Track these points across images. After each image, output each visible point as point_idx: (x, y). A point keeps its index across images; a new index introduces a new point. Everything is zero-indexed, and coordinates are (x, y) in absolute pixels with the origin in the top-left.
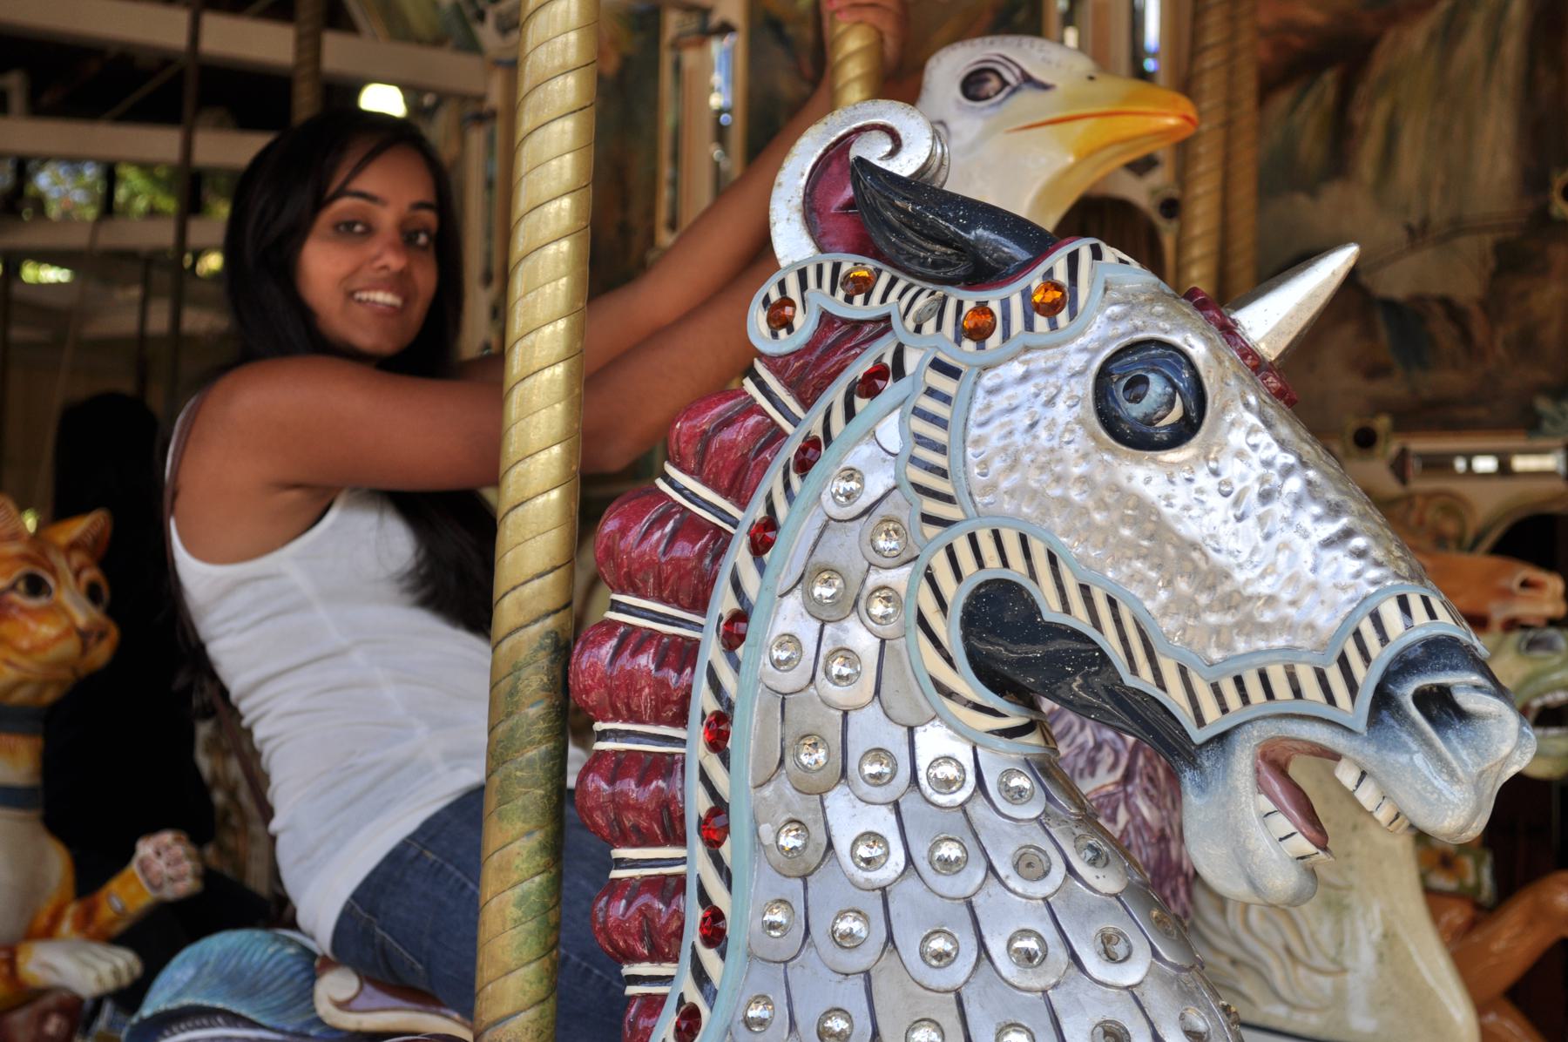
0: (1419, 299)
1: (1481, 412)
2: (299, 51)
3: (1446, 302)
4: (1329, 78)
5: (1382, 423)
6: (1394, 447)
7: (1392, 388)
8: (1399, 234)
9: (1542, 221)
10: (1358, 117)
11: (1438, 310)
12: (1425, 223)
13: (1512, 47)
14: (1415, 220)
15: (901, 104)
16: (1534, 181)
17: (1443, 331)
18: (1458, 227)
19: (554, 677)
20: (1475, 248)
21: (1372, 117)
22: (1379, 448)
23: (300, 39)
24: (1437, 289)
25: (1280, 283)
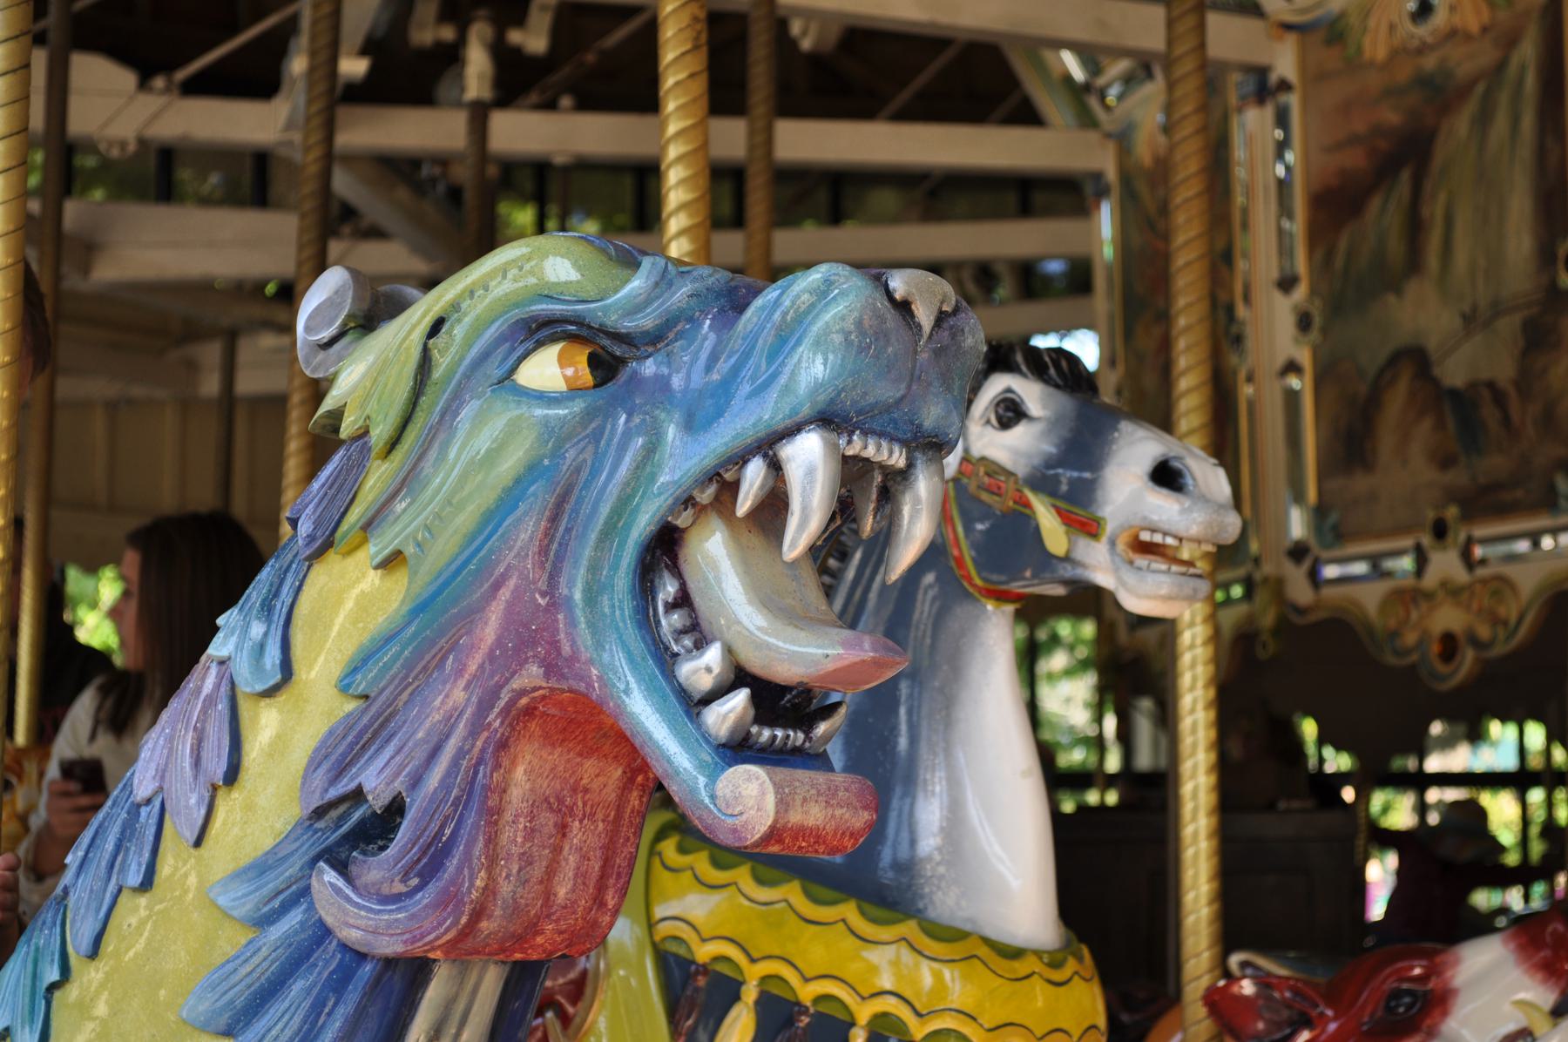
0: (1473, 385)
1: (1519, 493)
2: (751, 148)
3: (1491, 385)
4: (1405, 176)
5: (1452, 512)
6: (1462, 537)
7: (1458, 477)
8: (1457, 322)
9: (1553, 296)
10: (1425, 212)
11: (1486, 394)
12: (1474, 309)
13: (1528, 121)
14: (1466, 308)
15: (1085, 331)
16: (1546, 256)
17: (1489, 414)
18: (1498, 310)
19: (906, 794)
20: (1509, 326)
21: (1434, 211)
22: (1450, 538)
23: (751, 133)
24: (1485, 375)
25: (490, 1028)
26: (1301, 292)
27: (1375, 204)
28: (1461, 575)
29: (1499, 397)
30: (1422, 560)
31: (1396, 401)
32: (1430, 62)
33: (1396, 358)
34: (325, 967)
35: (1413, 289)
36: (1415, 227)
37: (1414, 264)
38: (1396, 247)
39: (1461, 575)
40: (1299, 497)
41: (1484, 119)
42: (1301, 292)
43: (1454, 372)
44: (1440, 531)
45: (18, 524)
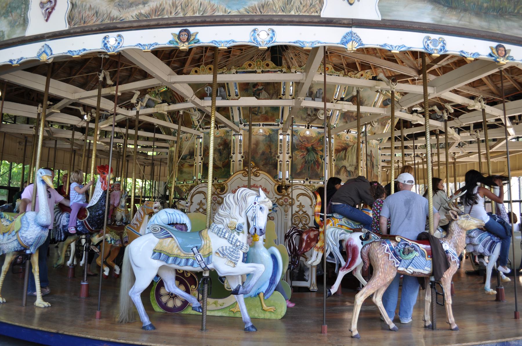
5: (308, 178)
13: (356, 151)
17: (351, 173)
21: (347, 155)
26: (242, 154)
27: (341, 152)
28: (309, 184)
29: (352, 172)
30: (304, 182)
31: (343, 170)
32: (347, 142)
33: (343, 166)
34: (332, 244)
35: (345, 161)
36: (345, 156)
37: (345, 159)
38: (343, 157)
39: (309, 184)
40: (200, 172)
41: (352, 149)
42: (242, 154)
43: (349, 169)
44: (307, 180)
45: (90, 50)
